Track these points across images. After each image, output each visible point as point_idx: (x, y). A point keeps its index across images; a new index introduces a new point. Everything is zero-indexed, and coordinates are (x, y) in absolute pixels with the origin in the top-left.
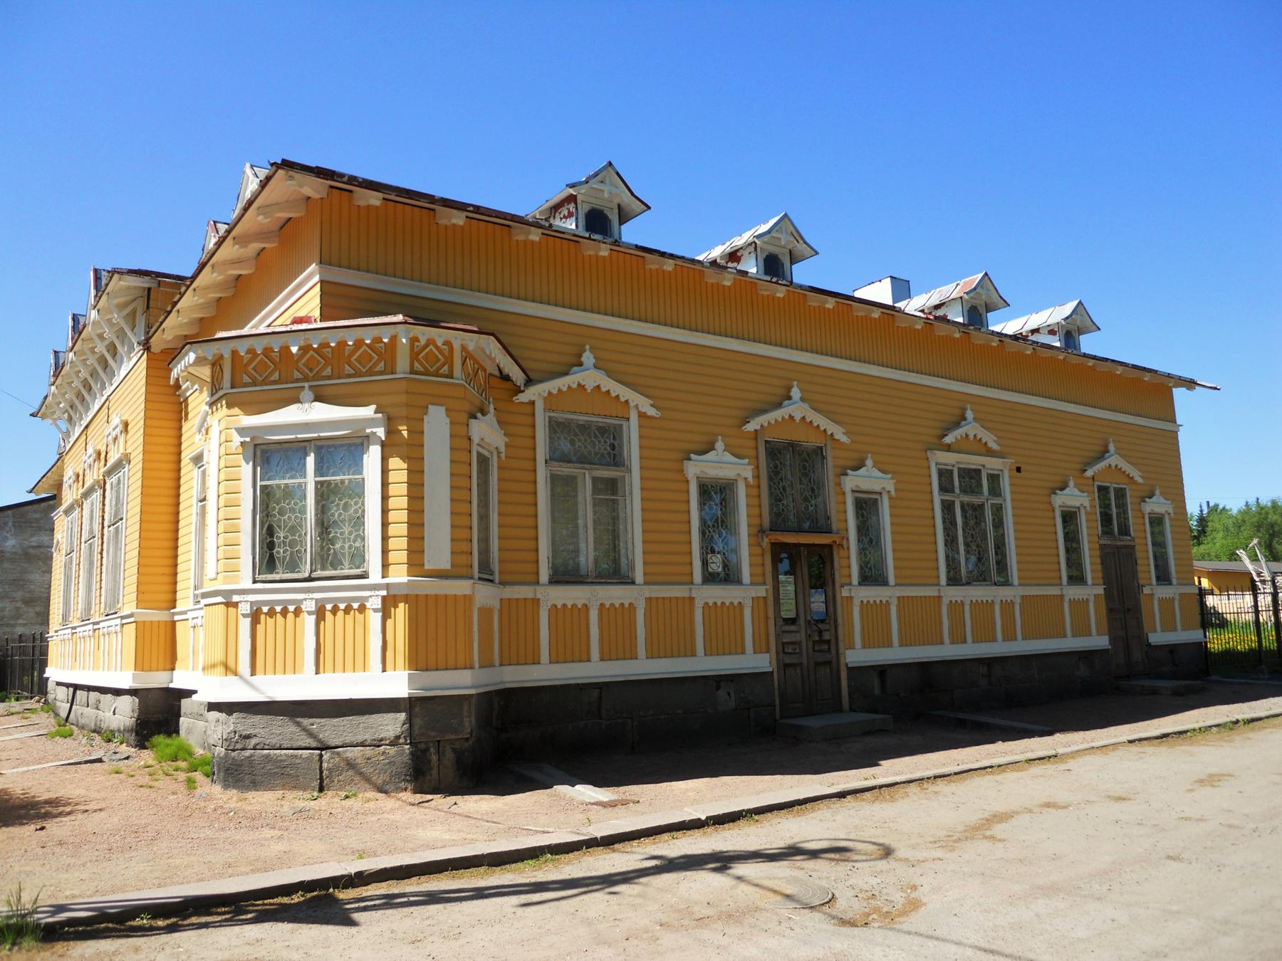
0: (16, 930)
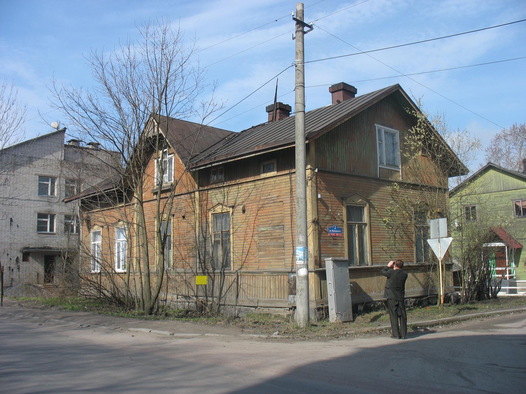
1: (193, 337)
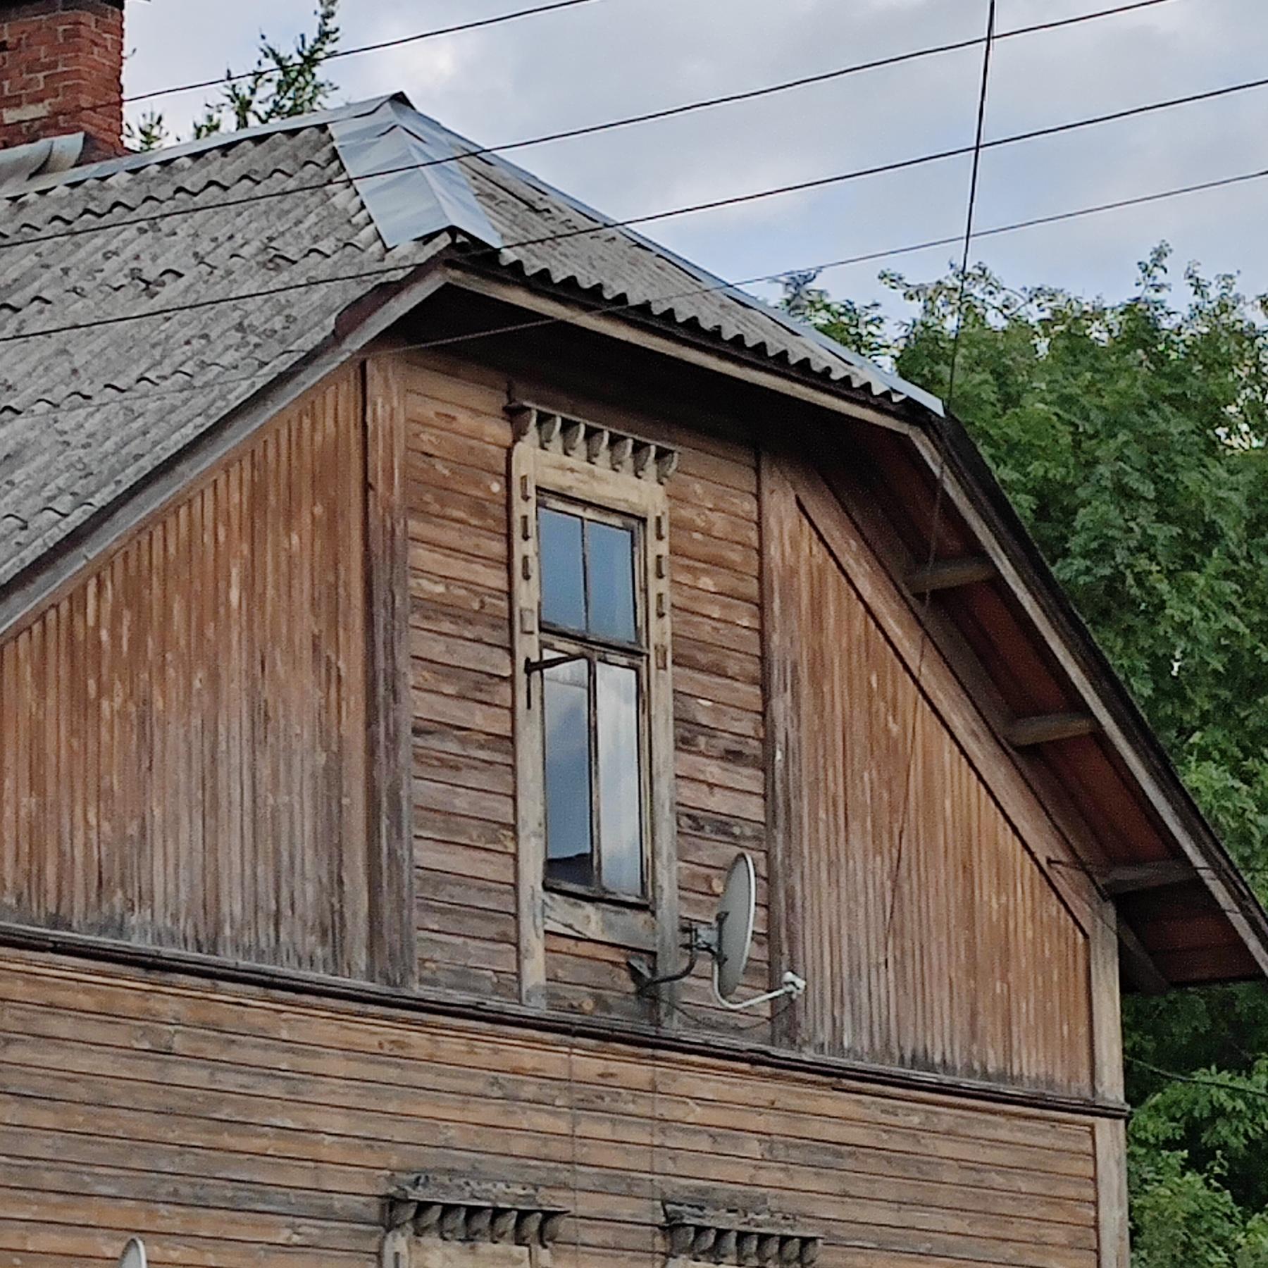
0: (3, 1000)
1: (841, 959)
